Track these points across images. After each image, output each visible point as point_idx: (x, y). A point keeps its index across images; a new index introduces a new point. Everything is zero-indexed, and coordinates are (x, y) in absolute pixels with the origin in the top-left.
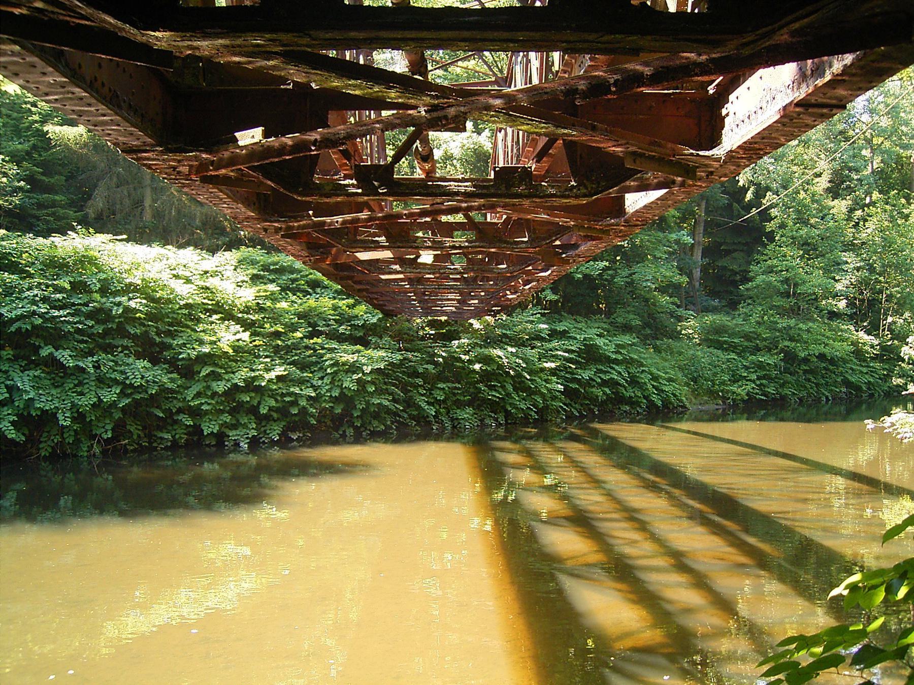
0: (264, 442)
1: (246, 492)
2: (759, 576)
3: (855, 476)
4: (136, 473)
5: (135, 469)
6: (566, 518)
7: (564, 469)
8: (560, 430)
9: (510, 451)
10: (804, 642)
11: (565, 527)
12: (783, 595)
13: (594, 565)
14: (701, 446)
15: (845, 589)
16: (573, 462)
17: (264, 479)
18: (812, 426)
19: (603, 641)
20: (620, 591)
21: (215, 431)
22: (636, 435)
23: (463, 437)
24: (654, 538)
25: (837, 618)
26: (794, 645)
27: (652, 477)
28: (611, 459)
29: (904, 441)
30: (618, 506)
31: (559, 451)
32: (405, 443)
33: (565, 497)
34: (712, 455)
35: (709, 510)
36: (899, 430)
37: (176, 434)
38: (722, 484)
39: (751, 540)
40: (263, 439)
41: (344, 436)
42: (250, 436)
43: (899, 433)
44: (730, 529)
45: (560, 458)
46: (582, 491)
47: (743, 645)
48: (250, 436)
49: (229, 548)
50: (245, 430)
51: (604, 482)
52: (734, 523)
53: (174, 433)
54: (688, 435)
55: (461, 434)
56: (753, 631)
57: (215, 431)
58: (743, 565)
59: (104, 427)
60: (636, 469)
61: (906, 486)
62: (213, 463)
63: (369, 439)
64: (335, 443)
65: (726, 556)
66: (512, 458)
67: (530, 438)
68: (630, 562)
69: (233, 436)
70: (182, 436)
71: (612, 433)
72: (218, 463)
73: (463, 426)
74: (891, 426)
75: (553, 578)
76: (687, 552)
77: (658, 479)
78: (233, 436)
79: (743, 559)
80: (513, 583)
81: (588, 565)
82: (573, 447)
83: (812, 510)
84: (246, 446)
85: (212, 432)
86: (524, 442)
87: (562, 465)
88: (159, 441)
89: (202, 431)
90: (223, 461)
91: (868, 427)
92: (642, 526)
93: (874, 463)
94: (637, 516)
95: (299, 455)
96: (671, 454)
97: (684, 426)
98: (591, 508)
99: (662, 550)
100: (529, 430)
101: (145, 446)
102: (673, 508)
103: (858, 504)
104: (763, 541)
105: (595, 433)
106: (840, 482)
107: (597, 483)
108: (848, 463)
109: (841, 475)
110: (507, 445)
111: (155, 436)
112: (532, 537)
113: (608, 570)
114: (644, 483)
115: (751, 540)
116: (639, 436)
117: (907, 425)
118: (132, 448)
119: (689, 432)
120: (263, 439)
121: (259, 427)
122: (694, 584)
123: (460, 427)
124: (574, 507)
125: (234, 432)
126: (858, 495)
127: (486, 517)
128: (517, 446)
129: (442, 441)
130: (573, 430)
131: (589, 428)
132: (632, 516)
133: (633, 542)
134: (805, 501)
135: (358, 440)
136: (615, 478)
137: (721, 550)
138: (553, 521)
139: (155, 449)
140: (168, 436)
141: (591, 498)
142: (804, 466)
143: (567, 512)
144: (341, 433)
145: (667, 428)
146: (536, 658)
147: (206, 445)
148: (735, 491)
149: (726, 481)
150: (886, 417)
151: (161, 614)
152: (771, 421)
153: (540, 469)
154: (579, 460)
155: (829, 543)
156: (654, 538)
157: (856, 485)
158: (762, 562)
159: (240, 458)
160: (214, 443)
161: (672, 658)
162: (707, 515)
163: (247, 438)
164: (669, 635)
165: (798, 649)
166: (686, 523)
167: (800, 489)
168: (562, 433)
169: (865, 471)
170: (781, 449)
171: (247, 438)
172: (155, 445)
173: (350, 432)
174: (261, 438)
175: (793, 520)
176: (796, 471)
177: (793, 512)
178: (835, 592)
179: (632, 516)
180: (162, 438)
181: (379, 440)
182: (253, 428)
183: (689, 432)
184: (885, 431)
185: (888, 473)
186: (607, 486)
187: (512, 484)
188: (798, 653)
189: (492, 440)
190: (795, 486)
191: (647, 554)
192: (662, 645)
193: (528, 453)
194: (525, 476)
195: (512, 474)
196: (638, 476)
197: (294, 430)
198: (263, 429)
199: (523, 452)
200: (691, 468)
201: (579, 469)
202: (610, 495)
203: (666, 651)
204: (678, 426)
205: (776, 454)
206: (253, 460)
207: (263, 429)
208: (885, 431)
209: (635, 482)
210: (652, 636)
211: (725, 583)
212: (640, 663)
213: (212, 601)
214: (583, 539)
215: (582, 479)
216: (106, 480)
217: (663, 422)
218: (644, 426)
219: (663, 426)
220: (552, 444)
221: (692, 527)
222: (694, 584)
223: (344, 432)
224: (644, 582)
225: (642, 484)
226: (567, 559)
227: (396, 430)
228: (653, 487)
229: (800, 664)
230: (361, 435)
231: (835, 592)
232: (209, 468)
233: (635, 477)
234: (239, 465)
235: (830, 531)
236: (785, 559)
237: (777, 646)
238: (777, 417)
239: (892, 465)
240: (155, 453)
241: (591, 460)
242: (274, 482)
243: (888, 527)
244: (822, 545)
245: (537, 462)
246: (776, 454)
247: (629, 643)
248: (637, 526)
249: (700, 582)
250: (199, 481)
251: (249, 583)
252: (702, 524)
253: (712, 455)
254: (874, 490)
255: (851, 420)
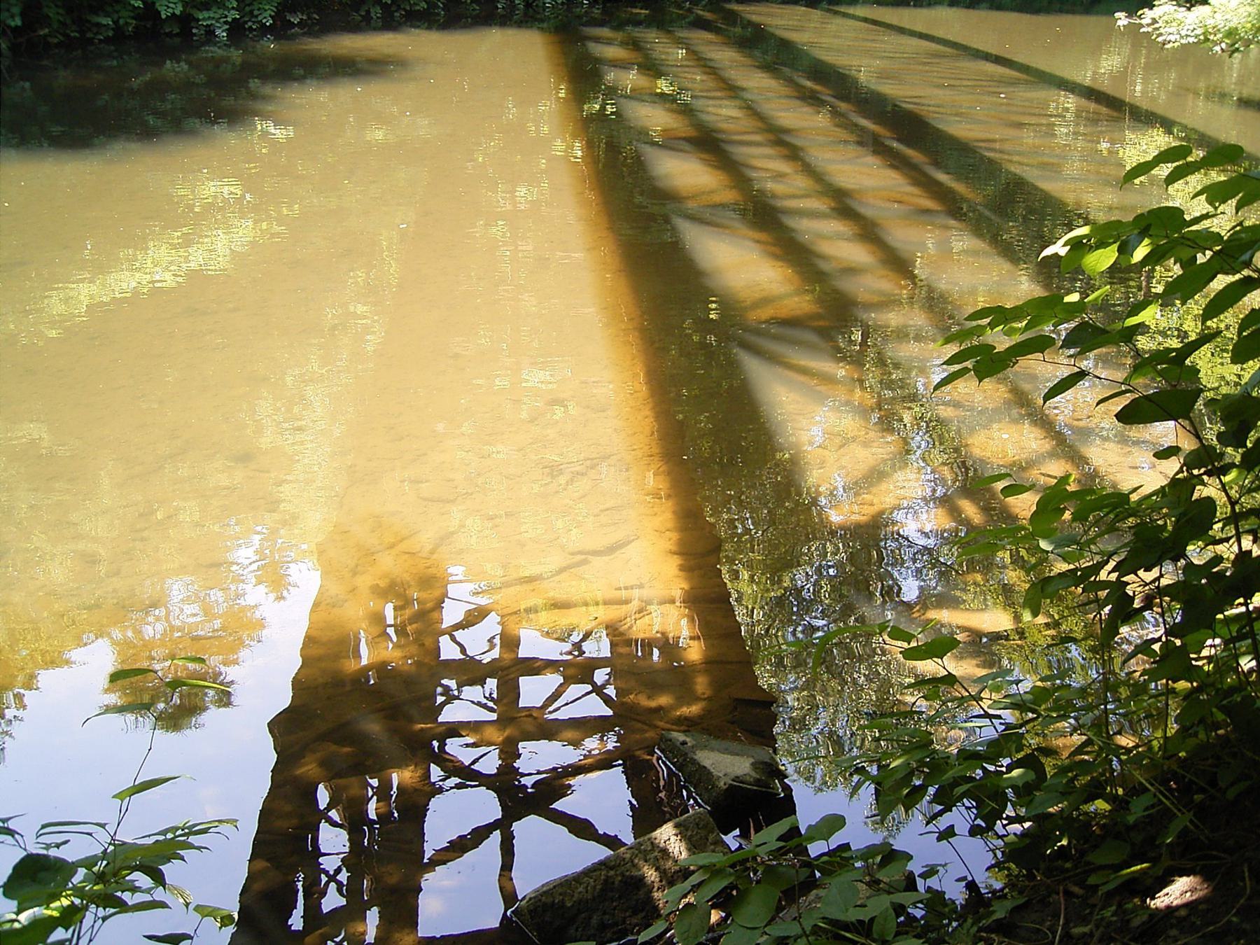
0: (250, 28)
1: (229, 102)
2: (947, 228)
3: (1091, 94)
4: (63, 78)
5: (62, 73)
6: (688, 140)
7: (687, 69)
8: (681, 12)
9: (609, 42)
10: (1000, 315)
11: (681, 151)
12: (975, 253)
13: (723, 206)
14: (883, 42)
15: (1064, 245)
16: (699, 59)
17: (254, 84)
18: (1041, 20)
19: (730, 306)
20: (758, 242)
21: (178, 12)
22: (791, 23)
23: (542, 21)
24: (809, 170)
25: (1047, 286)
26: (988, 320)
27: (809, 84)
28: (750, 56)
29: (1166, 46)
30: (760, 124)
31: (680, 43)
32: (455, 29)
33: (687, 111)
34: (897, 55)
35: (888, 134)
36: (1162, 30)
37: (119, 18)
38: (906, 97)
39: (942, 177)
40: (250, 24)
41: (367, 18)
42: (229, 19)
43: (1161, 35)
44: (915, 161)
45: (682, 53)
46: (711, 102)
47: (918, 319)
48: (229, 19)
49: (214, 188)
50: (221, 11)
51: (743, 89)
52: (921, 153)
53: (116, 16)
54: (863, 24)
55: (538, 16)
56: (935, 303)
57: (178, 12)
58: (927, 212)
59: (8, 10)
60: (786, 70)
61: (1160, 111)
62: (178, 62)
63: (405, 23)
64: (355, 28)
65: (905, 198)
66: (613, 52)
67: (638, 23)
68: (772, 202)
69: (204, 19)
70: (130, 21)
71: (755, 18)
72: (187, 62)
73: (541, 4)
74: (1153, 24)
75: (667, 220)
76: (853, 190)
77: (818, 88)
78: (204, 19)
79: (929, 204)
80: (611, 229)
81: (715, 206)
82: (700, 37)
83: (1029, 138)
84: (225, 34)
85: (174, 14)
86: (629, 28)
87: (684, 63)
88: (95, 30)
89: (159, 13)
90: (193, 58)
91: (1120, 23)
92: (794, 154)
93: (1122, 76)
94: (788, 138)
95: (305, 47)
96: (838, 51)
97: (860, 11)
98: (724, 126)
99: (818, 188)
100: (638, 11)
101: (75, 37)
102: (836, 129)
103: (1092, 134)
104: (958, 180)
105: (732, 18)
106: (1070, 102)
107: (732, 90)
108: (1086, 78)
109: (1073, 92)
110: (605, 32)
111: (88, 21)
112: (639, 164)
113: (743, 213)
114: (799, 92)
115: (942, 177)
116: (795, 23)
117: (1174, 24)
118: (56, 41)
119: (866, 20)
120: (250, 24)
121: (242, 5)
122: (859, 235)
123: (537, 6)
124: (700, 126)
125: (206, 14)
126: (1094, 120)
127: (574, 137)
128: (619, 36)
129: (511, 26)
130: (701, 13)
131: (723, 10)
132: (780, 139)
133: (779, 176)
134: (1020, 125)
135: (389, 24)
136: (757, 83)
137: (902, 190)
138: (670, 143)
139: (90, 41)
140: (108, 21)
141: (724, 112)
142: (1024, 76)
143: (690, 132)
144: (363, 13)
145: (836, 13)
146: (642, 331)
147: (165, 33)
148: (926, 108)
149: (914, 94)
150: (1146, 10)
151: (124, 282)
152: (983, 9)
153: (653, 69)
154: (739, 84)
155: (1049, 186)
156: (809, 170)
157: (1092, 106)
158: (954, 207)
159: (218, 52)
160: (176, 30)
161: (826, 334)
162: (882, 140)
163: (226, 23)
164: (820, 301)
165: (992, 325)
166: (853, 150)
167: (1015, 109)
168: (683, 17)
169: (1106, 86)
170: (993, 51)
171: (226, 23)
172: (90, 35)
173: (376, 12)
174: (246, 22)
175: (1001, 152)
176: (1014, 83)
177: (1001, 140)
178: (1048, 251)
179: (780, 139)
180: (98, 25)
181: (419, 24)
182: (233, 8)
183: (866, 20)
184: (1142, 30)
185: (1137, 91)
186: (747, 96)
187: (612, 92)
188: (992, 330)
189: (584, 25)
190: (1008, 105)
191: (798, 193)
192: (818, 317)
193: (635, 45)
194: (631, 79)
195: (611, 76)
196: (790, 81)
197: (293, 11)
198: (247, 9)
199: (627, 44)
200: (866, 72)
201: (708, 70)
202: (752, 110)
203: (816, 324)
204: (850, 10)
205: (987, 57)
206: (236, 55)
207: (247, 9)
208: (1142, 30)
209: (785, 90)
210: (801, 304)
211: (902, 235)
212: (776, 338)
213: (197, 257)
214: (710, 170)
215: (711, 84)
216: (21, 90)
217: (830, 3)
218: (804, 8)
219: (828, 11)
220: (669, 32)
221: (865, 156)
222: (859, 235)
223: (368, 12)
224: (793, 230)
225: (796, 94)
226: (688, 198)
227: (443, 9)
228: (812, 99)
229: (995, 348)
230: (392, 17)
231: (1048, 251)
232: (174, 69)
233: (786, 84)
234: (218, 62)
235: (1052, 169)
236: (986, 206)
237: (966, 319)
238: (991, 5)
239: (1145, 81)
240: (92, 48)
241: (725, 56)
242: (267, 89)
243: (1128, 168)
244: (1036, 188)
245: (647, 57)
246: (987, 57)
247: (766, 313)
248: (786, 152)
249: (869, 232)
250: (159, 88)
251: (245, 231)
252: (875, 152)
253: (897, 55)
254: (1115, 114)
255: (1097, 13)
